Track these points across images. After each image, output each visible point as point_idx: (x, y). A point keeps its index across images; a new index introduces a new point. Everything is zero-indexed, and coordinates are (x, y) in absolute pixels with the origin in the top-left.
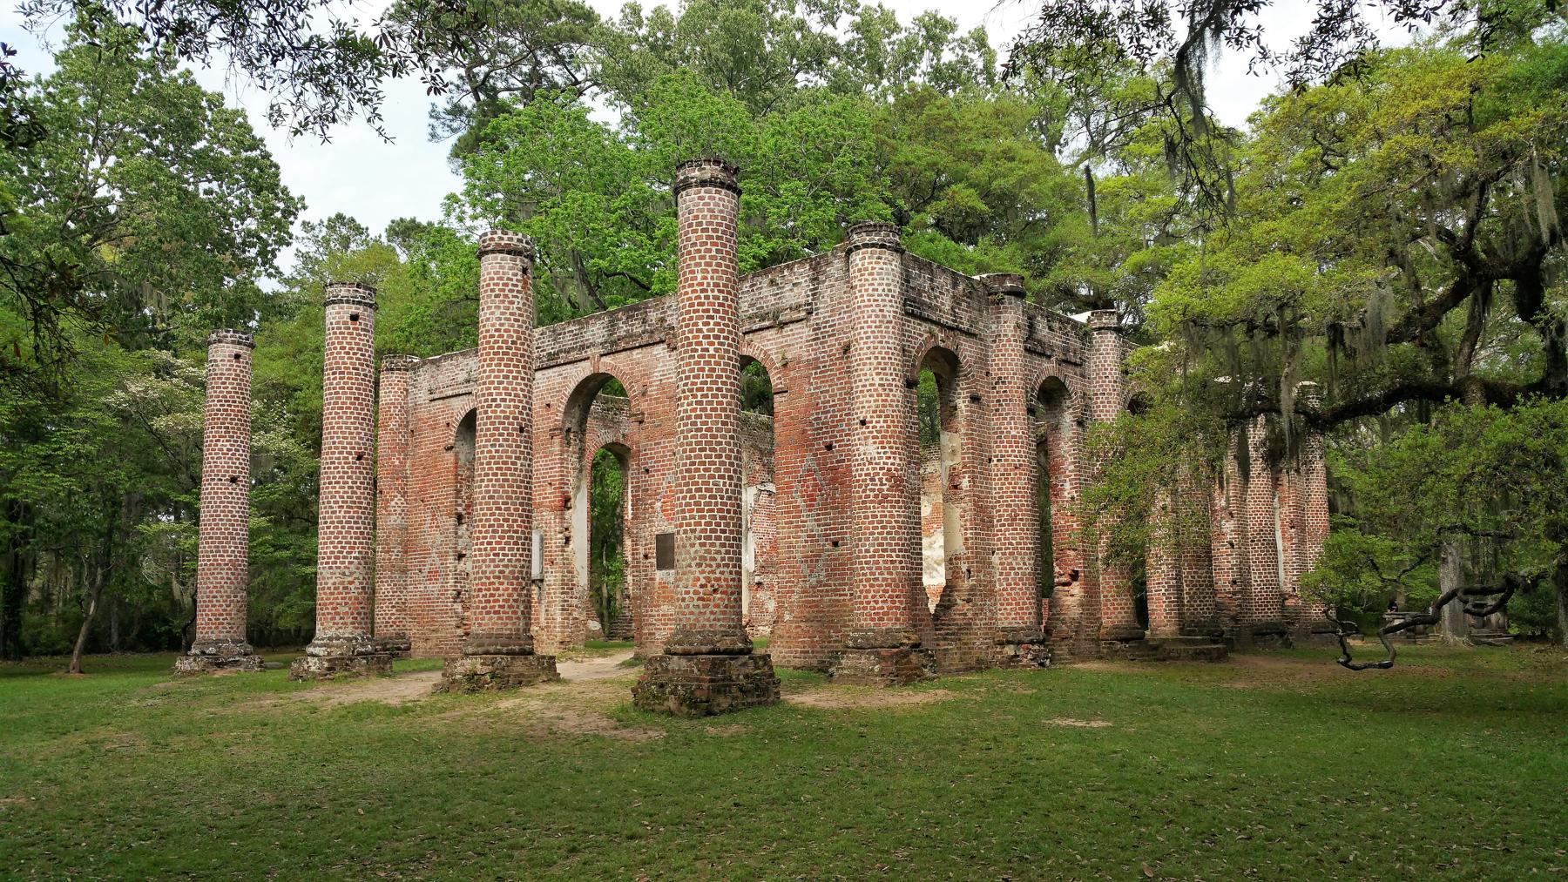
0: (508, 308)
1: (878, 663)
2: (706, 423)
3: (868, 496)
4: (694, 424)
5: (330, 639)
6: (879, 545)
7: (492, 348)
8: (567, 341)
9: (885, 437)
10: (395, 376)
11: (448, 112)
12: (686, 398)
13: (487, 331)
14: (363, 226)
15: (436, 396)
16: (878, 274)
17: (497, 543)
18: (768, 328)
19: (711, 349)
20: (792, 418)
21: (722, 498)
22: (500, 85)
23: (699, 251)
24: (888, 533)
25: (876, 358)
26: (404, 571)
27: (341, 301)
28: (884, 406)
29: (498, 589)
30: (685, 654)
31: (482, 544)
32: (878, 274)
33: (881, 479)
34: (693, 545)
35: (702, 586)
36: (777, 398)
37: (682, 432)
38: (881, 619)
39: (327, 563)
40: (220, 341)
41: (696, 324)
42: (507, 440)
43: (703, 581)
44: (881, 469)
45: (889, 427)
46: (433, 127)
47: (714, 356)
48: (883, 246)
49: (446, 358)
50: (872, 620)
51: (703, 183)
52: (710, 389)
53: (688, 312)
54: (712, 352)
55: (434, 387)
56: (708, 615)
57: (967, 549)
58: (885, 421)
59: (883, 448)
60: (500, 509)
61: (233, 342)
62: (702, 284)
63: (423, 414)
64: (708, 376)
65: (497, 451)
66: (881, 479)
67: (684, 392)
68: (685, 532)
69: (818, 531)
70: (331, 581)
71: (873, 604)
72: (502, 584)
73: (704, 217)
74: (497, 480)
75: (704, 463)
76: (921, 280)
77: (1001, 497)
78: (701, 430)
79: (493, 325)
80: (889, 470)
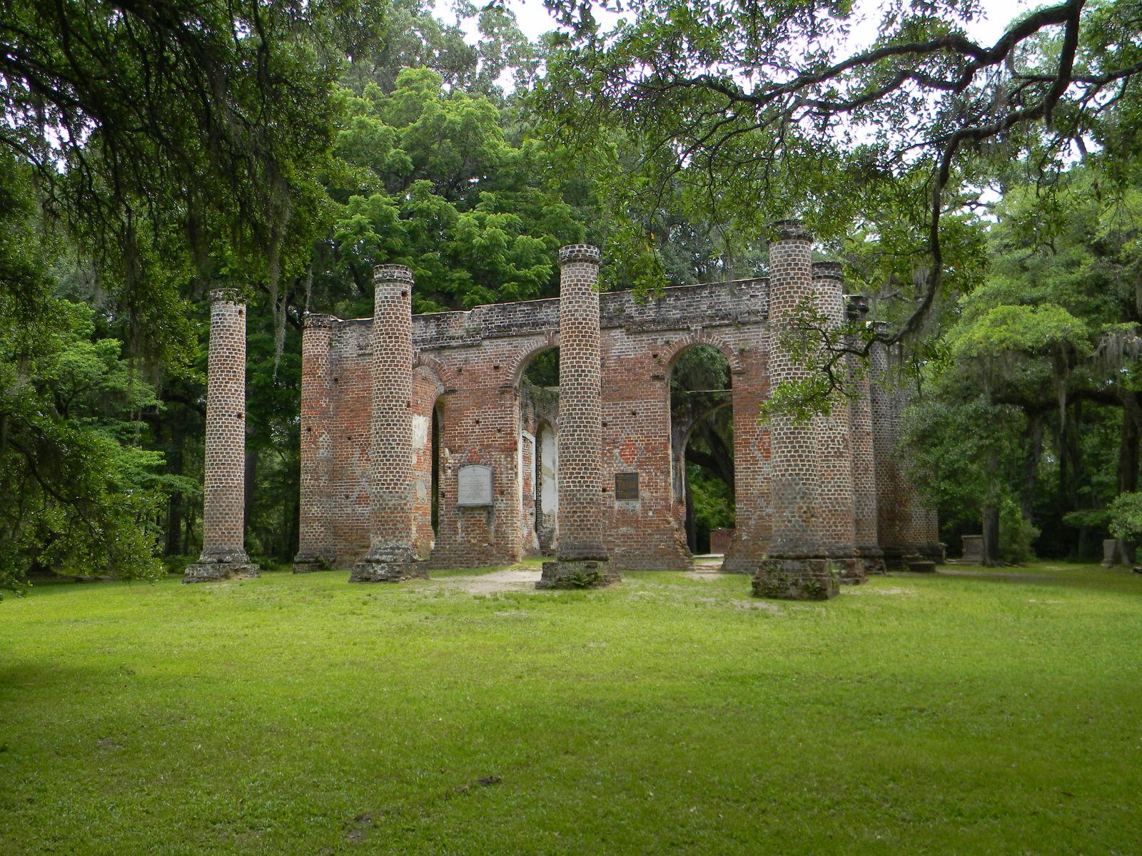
3: (829, 452)
5: (392, 548)
8: (519, 317)
10: (322, 333)
17: (589, 477)
18: (727, 326)
27: (396, 280)
30: (798, 558)
34: (797, 484)
35: (805, 512)
39: (387, 488)
43: (805, 509)
51: (799, 237)
60: (589, 452)
70: (391, 503)
73: (799, 260)
79: (581, 315)
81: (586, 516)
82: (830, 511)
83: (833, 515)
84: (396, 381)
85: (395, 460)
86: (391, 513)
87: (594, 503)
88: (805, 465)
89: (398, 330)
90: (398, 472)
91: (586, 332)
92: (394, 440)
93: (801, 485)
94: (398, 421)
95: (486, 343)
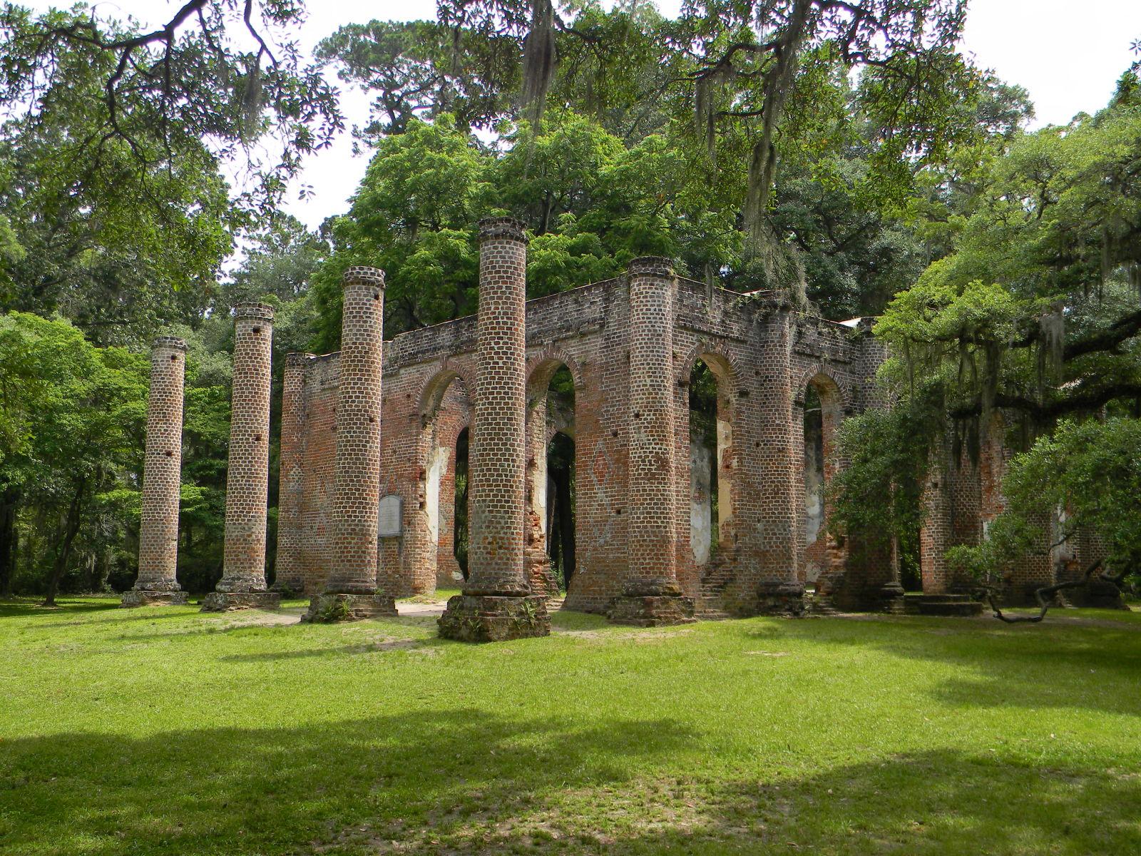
0: (362, 326)
1: (643, 607)
2: (495, 419)
3: (640, 474)
4: (487, 419)
5: (233, 579)
6: (648, 513)
7: (350, 357)
8: (424, 344)
9: (654, 427)
10: (295, 371)
11: (366, 131)
12: (482, 399)
13: (347, 344)
14: (303, 223)
15: (326, 386)
16: (651, 297)
17: (350, 507)
18: (572, 337)
19: (501, 362)
20: (588, 410)
21: (506, 476)
22: (413, 103)
23: (493, 288)
24: (655, 504)
25: (648, 364)
26: (300, 527)
28: (654, 402)
29: (350, 543)
31: (339, 507)
32: (651, 297)
33: (650, 461)
35: (489, 543)
36: (578, 395)
37: (478, 425)
38: (648, 573)
40: (161, 346)
41: (489, 344)
42: (359, 428)
43: (490, 540)
44: (650, 452)
45: (657, 419)
46: (355, 144)
47: (502, 368)
48: (655, 275)
49: (333, 356)
50: (641, 573)
51: (497, 236)
52: (499, 393)
53: (484, 334)
54: (501, 365)
55: (324, 379)
56: (494, 565)
57: (735, 517)
58: (654, 415)
59: (652, 436)
60: (352, 481)
61: (170, 346)
62: (495, 313)
63: (316, 400)
64: (497, 383)
65: (352, 437)
66: (650, 461)
67: (480, 395)
68: (479, 501)
69: (606, 501)
70: (234, 534)
71: (642, 560)
72: (353, 539)
73: (497, 262)
74: (351, 459)
75: (493, 450)
76: (694, 299)
77: (767, 475)
78: (491, 424)
80: (657, 453)
81: (346, 548)
82: (638, 541)
83: (641, 546)
84: (243, 416)
85: (239, 493)
86: (235, 544)
87: (355, 534)
88: (492, 490)
89: (248, 365)
90: (242, 504)
91: (356, 357)
92: (239, 473)
93: (487, 513)
94: (244, 454)
95: (402, 371)
